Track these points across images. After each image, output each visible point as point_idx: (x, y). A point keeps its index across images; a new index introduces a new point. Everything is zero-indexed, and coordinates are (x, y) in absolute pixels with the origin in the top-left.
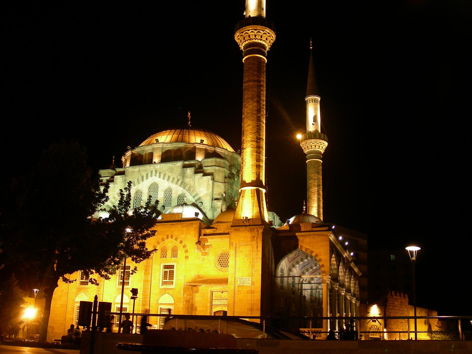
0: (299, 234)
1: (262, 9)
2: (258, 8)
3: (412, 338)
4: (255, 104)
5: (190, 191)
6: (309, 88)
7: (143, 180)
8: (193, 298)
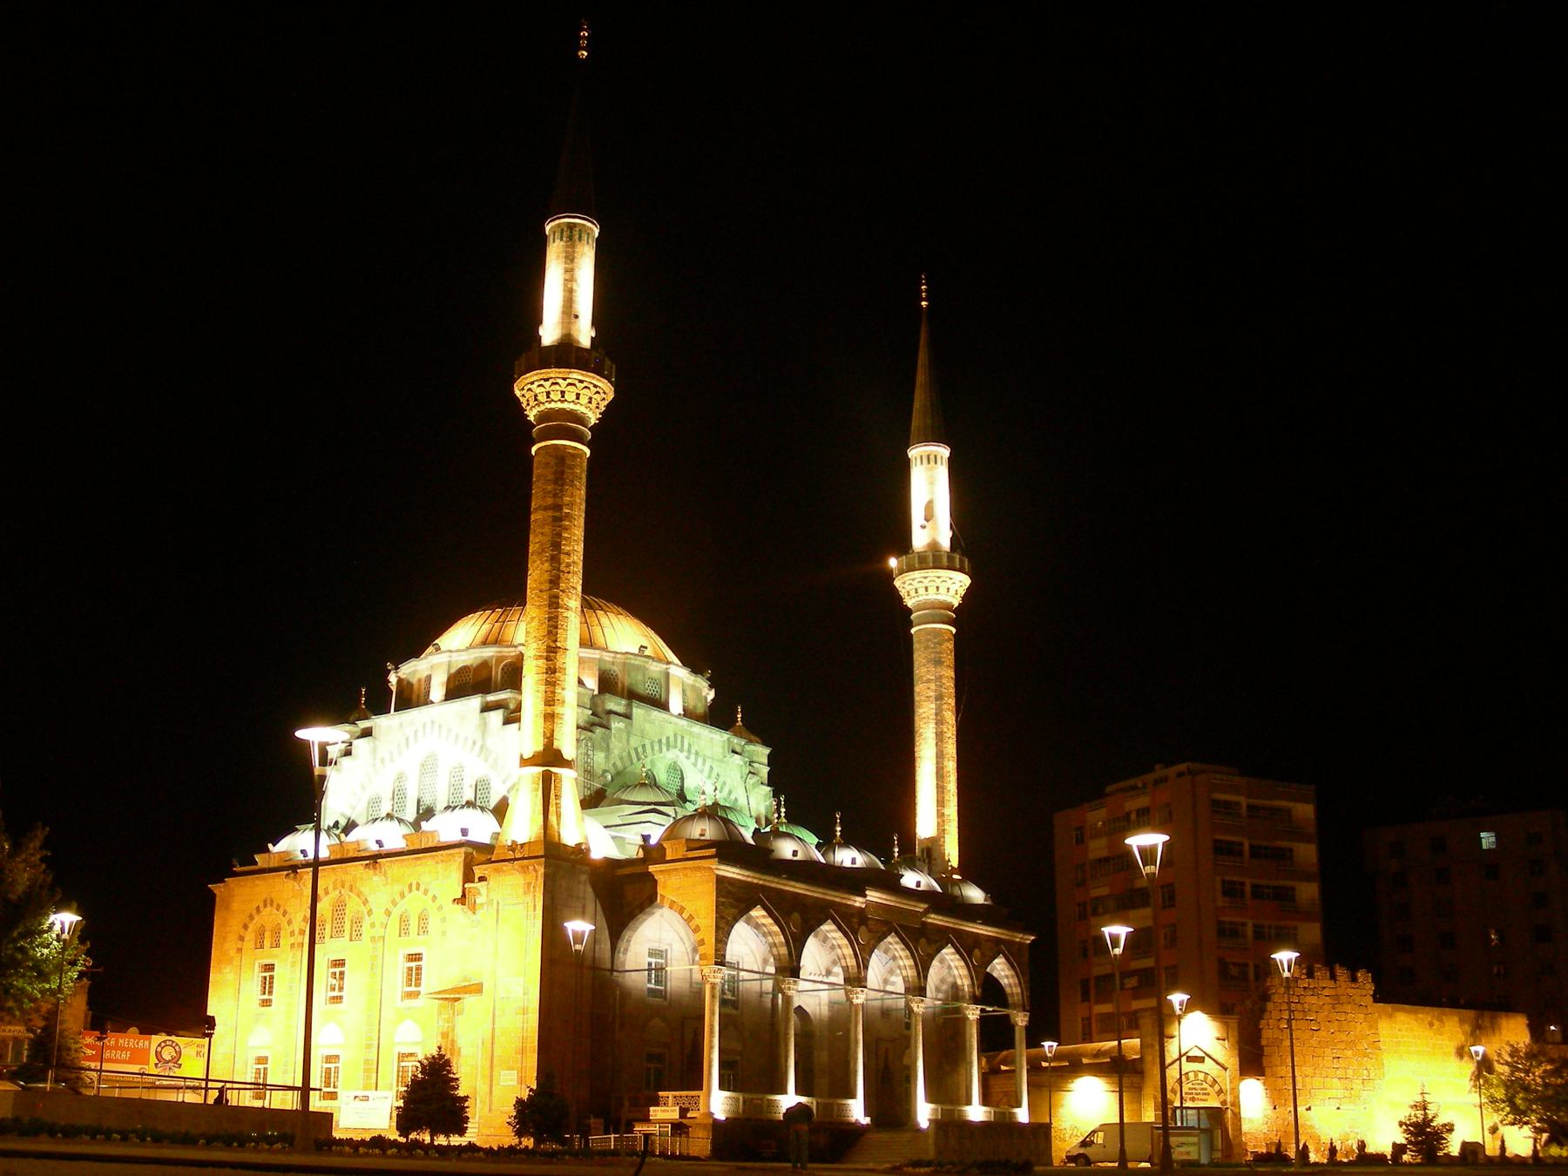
0: (654, 869)
1: (572, 317)
4: (547, 565)
6: (916, 423)
7: (330, 765)
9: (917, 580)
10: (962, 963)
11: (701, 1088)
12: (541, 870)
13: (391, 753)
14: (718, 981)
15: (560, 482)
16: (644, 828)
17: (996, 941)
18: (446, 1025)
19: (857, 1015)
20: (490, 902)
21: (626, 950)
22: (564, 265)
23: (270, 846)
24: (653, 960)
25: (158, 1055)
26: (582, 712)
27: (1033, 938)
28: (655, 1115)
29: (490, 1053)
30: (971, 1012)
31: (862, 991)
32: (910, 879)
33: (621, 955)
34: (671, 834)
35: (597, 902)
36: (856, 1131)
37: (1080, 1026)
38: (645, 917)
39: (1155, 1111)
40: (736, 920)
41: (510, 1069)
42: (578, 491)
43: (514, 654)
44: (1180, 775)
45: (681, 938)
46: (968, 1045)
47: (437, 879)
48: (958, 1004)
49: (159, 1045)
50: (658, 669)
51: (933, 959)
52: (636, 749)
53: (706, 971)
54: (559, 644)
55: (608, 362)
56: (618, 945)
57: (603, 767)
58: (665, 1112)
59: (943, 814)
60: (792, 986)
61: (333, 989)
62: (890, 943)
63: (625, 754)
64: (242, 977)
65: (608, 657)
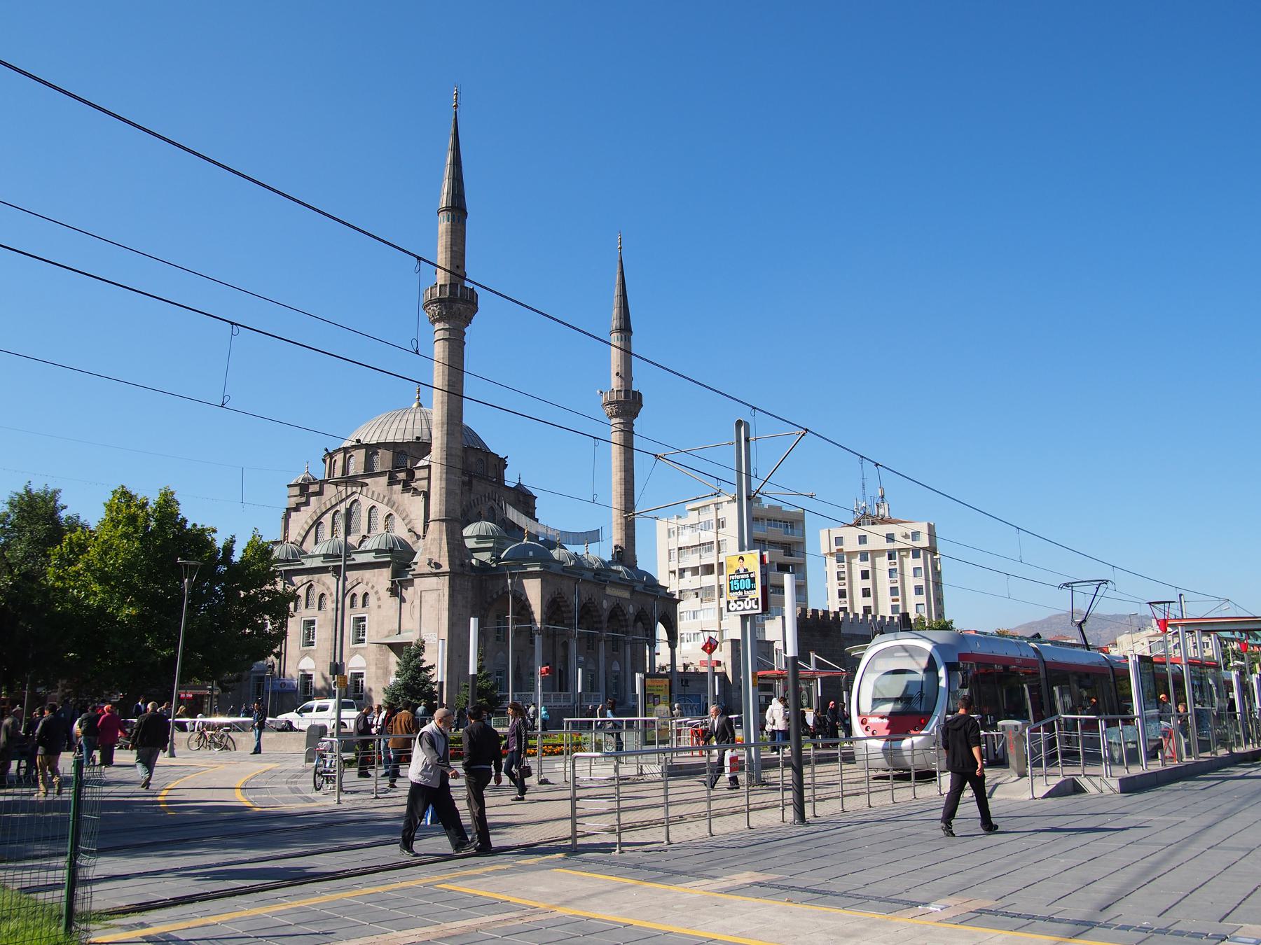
3: (686, 666)
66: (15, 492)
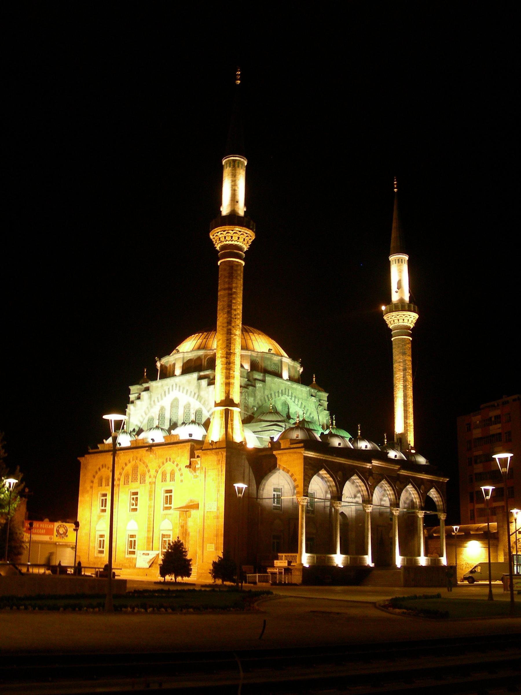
0: (275, 453)
1: (236, 202)
2: (231, 203)
4: (226, 316)
5: (205, 405)
6: (392, 245)
8: (186, 523)
9: (394, 316)
10: (416, 492)
11: (297, 553)
12: (225, 454)
13: (158, 398)
14: (305, 504)
15: (231, 278)
16: (271, 432)
17: (431, 481)
18: (183, 522)
19: (368, 517)
20: (201, 468)
21: (263, 489)
22: (231, 179)
23: (104, 441)
24: (275, 493)
25: (58, 531)
26: (243, 380)
27: (448, 479)
28: (277, 564)
29: (202, 536)
30: (420, 514)
31: (370, 506)
32: (392, 454)
33: (261, 491)
34: (283, 437)
35: (250, 468)
36: (368, 568)
37: (469, 513)
38: (272, 474)
39: (504, 556)
40: (313, 476)
41: (211, 543)
42: (239, 282)
43: (212, 353)
44: (514, 400)
45: (288, 483)
46: (419, 529)
47: (179, 456)
48: (414, 511)
49: (58, 527)
50: (277, 359)
51: (402, 491)
52: (268, 396)
53: (299, 499)
54: (231, 351)
55: (252, 222)
56: (260, 486)
57: (253, 404)
58: (281, 563)
59: (407, 422)
60: (338, 505)
61: (133, 505)
62: (383, 484)
63: (262, 398)
64: (93, 499)
65: (254, 354)
66: (181, 423)
